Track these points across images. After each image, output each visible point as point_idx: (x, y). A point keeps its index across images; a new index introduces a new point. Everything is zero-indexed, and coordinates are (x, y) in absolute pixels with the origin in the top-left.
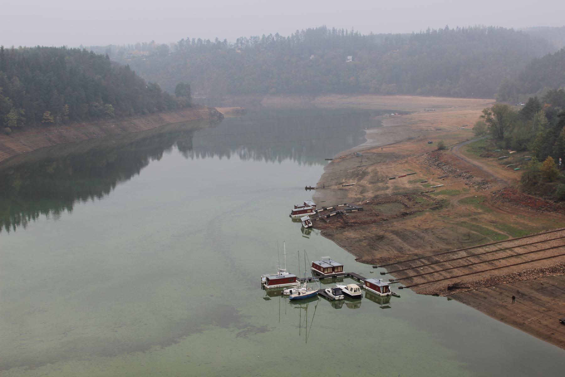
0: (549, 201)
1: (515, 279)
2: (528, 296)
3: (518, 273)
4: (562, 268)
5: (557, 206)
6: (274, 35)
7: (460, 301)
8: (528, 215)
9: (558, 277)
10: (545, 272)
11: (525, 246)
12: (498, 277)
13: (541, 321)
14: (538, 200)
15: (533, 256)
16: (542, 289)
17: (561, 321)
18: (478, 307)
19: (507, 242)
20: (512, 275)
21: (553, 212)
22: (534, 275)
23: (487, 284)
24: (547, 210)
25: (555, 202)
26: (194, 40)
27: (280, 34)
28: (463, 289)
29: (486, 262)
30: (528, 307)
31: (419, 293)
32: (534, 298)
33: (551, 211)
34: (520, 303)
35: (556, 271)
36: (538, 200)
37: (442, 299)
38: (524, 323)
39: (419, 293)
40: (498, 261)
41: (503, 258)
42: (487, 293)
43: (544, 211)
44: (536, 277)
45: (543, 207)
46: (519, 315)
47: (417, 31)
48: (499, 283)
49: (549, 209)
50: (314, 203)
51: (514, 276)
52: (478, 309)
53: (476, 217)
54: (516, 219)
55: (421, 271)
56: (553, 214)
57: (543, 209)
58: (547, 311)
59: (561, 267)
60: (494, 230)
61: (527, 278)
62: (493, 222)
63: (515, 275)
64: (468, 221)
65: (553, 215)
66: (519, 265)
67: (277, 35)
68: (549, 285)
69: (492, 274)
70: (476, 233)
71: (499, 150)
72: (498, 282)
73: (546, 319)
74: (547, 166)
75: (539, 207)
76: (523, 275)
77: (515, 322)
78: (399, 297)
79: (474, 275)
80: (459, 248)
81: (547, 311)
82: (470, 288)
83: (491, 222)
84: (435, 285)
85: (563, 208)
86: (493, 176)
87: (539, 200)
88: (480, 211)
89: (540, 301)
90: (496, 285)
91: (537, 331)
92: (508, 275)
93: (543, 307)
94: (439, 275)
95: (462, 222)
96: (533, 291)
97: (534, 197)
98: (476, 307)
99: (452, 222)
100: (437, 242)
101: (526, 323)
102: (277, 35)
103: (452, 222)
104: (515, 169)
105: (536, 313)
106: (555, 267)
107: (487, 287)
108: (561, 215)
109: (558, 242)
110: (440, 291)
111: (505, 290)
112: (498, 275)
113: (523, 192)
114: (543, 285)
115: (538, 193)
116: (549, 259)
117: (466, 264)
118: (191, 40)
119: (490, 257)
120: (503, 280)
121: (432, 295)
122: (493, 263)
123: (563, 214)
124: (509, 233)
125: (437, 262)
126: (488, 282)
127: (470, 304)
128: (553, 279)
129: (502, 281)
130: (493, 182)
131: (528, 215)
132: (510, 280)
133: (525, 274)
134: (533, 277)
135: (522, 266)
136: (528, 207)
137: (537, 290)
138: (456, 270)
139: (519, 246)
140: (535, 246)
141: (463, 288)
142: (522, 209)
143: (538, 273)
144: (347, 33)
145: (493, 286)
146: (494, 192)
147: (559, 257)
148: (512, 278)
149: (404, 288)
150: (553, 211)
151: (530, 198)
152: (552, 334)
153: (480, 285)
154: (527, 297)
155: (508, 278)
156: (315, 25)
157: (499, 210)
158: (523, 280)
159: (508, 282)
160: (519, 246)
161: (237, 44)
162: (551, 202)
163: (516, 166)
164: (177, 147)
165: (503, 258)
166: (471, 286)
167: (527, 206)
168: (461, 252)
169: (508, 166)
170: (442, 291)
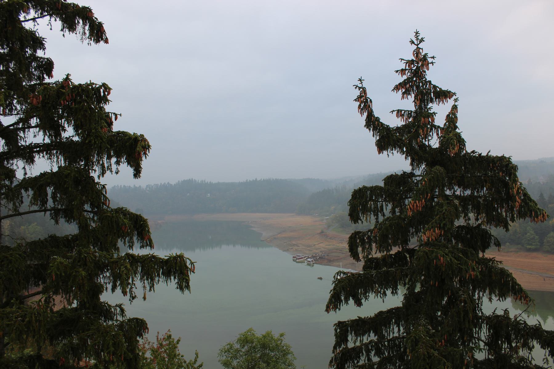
6: (166, 183)
26: (121, 186)
27: (170, 183)
47: (241, 181)
48: (424, 360)
50: (349, 300)
67: (168, 183)
102: (168, 183)
118: (119, 186)
144: (205, 182)
156: (187, 178)
161: (147, 188)
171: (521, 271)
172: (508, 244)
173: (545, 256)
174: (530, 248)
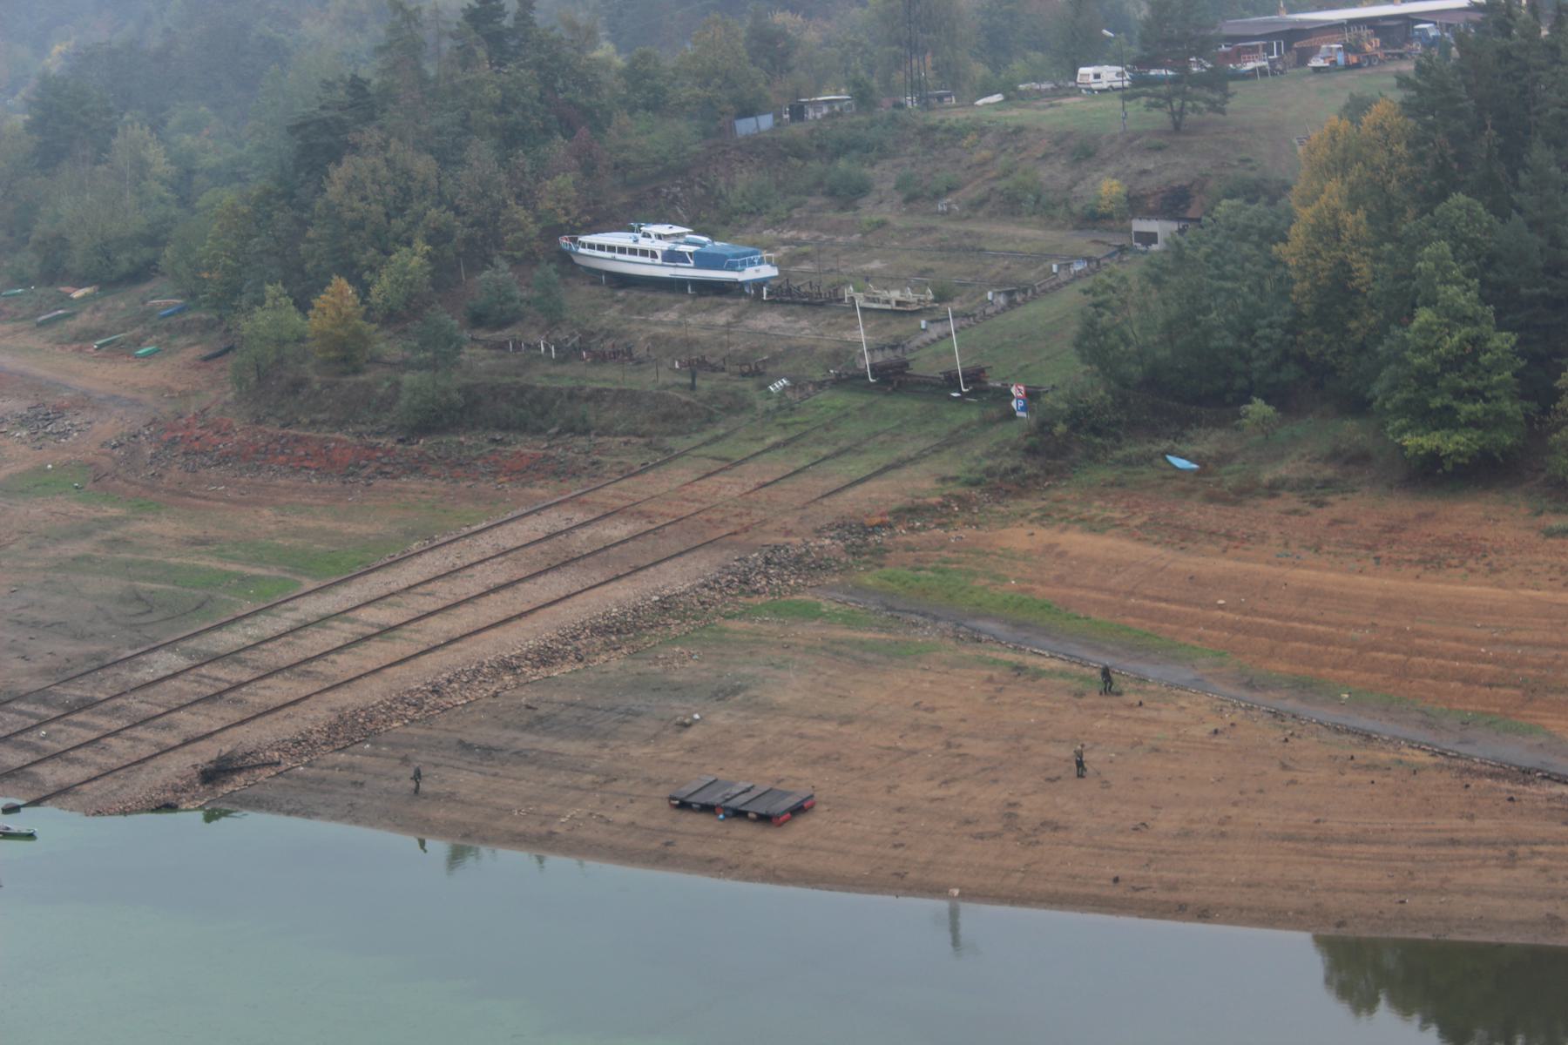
0: (378, 441)
1: (426, 707)
2: (507, 750)
3: (430, 687)
4: (569, 648)
5: (416, 455)
7: (269, 810)
8: (319, 501)
9: (571, 677)
10: (519, 667)
11: (390, 599)
12: (362, 710)
13: (607, 814)
14: (333, 444)
15: (440, 627)
16: (538, 722)
17: (675, 799)
18: (352, 814)
19: (313, 597)
20: (412, 696)
21: (408, 478)
22: (486, 686)
23: (334, 739)
24: (381, 473)
25: (401, 441)
28: (257, 772)
29: (280, 671)
30: (531, 784)
31: (99, 812)
32: (534, 753)
33: (399, 477)
34: (495, 775)
35: (554, 658)
36: (333, 444)
37: (189, 820)
38: (551, 833)
39: (99, 812)
40: (324, 663)
41: (338, 650)
42: (351, 767)
43: (374, 477)
44: (494, 689)
45: (364, 467)
46: (519, 811)
49: (387, 469)
51: (421, 698)
52: (357, 822)
53: (117, 533)
54: (281, 518)
55: (47, 743)
56: (413, 484)
57: (366, 472)
58: (605, 782)
59: (566, 644)
60: (224, 568)
61: (466, 698)
62: (196, 542)
63: (421, 692)
64: (96, 550)
65: (414, 486)
66: (413, 662)
68: (555, 705)
69: (337, 705)
70: (159, 586)
71: (20, 290)
72: (370, 726)
73: (618, 807)
74: (334, 314)
75: (348, 467)
76: (448, 690)
77: (519, 835)
78: (30, 836)
79: (269, 718)
80: (141, 644)
81: (605, 782)
82: (278, 763)
83: (193, 544)
84: (143, 776)
85: (440, 457)
86: (67, 387)
87: (337, 441)
88: (114, 512)
89: (561, 758)
90: (368, 736)
91: (611, 847)
92: (395, 699)
93: (587, 773)
94: (128, 743)
95: (74, 559)
96: (516, 734)
97: (311, 433)
98: (346, 816)
99: (33, 564)
100: (31, 638)
101: (556, 828)
103: (33, 564)
104: (140, 352)
105: (571, 794)
106: (545, 645)
107: (339, 750)
108: (444, 483)
109: (500, 567)
110: (176, 791)
111: (413, 746)
112: (360, 703)
113: (258, 422)
114: (535, 709)
115: (320, 417)
116: (508, 627)
117: (211, 692)
119: (557, 584)
120: (384, 717)
121: (153, 811)
122: (309, 672)
123: (450, 480)
124: (288, 568)
125: (87, 705)
126: (337, 734)
127: (317, 814)
128: (559, 685)
129: (385, 721)
130: (83, 407)
131: (319, 501)
132: (409, 713)
133: (456, 686)
134: (486, 690)
135: (428, 661)
136: (304, 471)
137: (528, 727)
138: (182, 714)
139: (368, 603)
140: (429, 594)
141: (256, 766)
142: (282, 482)
143: (496, 675)
145: (360, 741)
146: (114, 443)
147: (540, 612)
148: (415, 705)
149: (24, 806)
150: (404, 473)
151: (298, 440)
152: (668, 844)
153: (311, 745)
154: (506, 754)
155: (401, 707)
157: (188, 499)
158: (457, 705)
159: (406, 721)
160: (368, 603)
162: (386, 442)
163: (139, 343)
164: (738, 132)
165: (338, 650)
166: (281, 756)
167: (299, 471)
168: (155, 656)
169: (100, 347)
170: (184, 791)
171: (1290, 704)
172: (1258, 408)
173: (1550, 533)
174: (1433, 459)
